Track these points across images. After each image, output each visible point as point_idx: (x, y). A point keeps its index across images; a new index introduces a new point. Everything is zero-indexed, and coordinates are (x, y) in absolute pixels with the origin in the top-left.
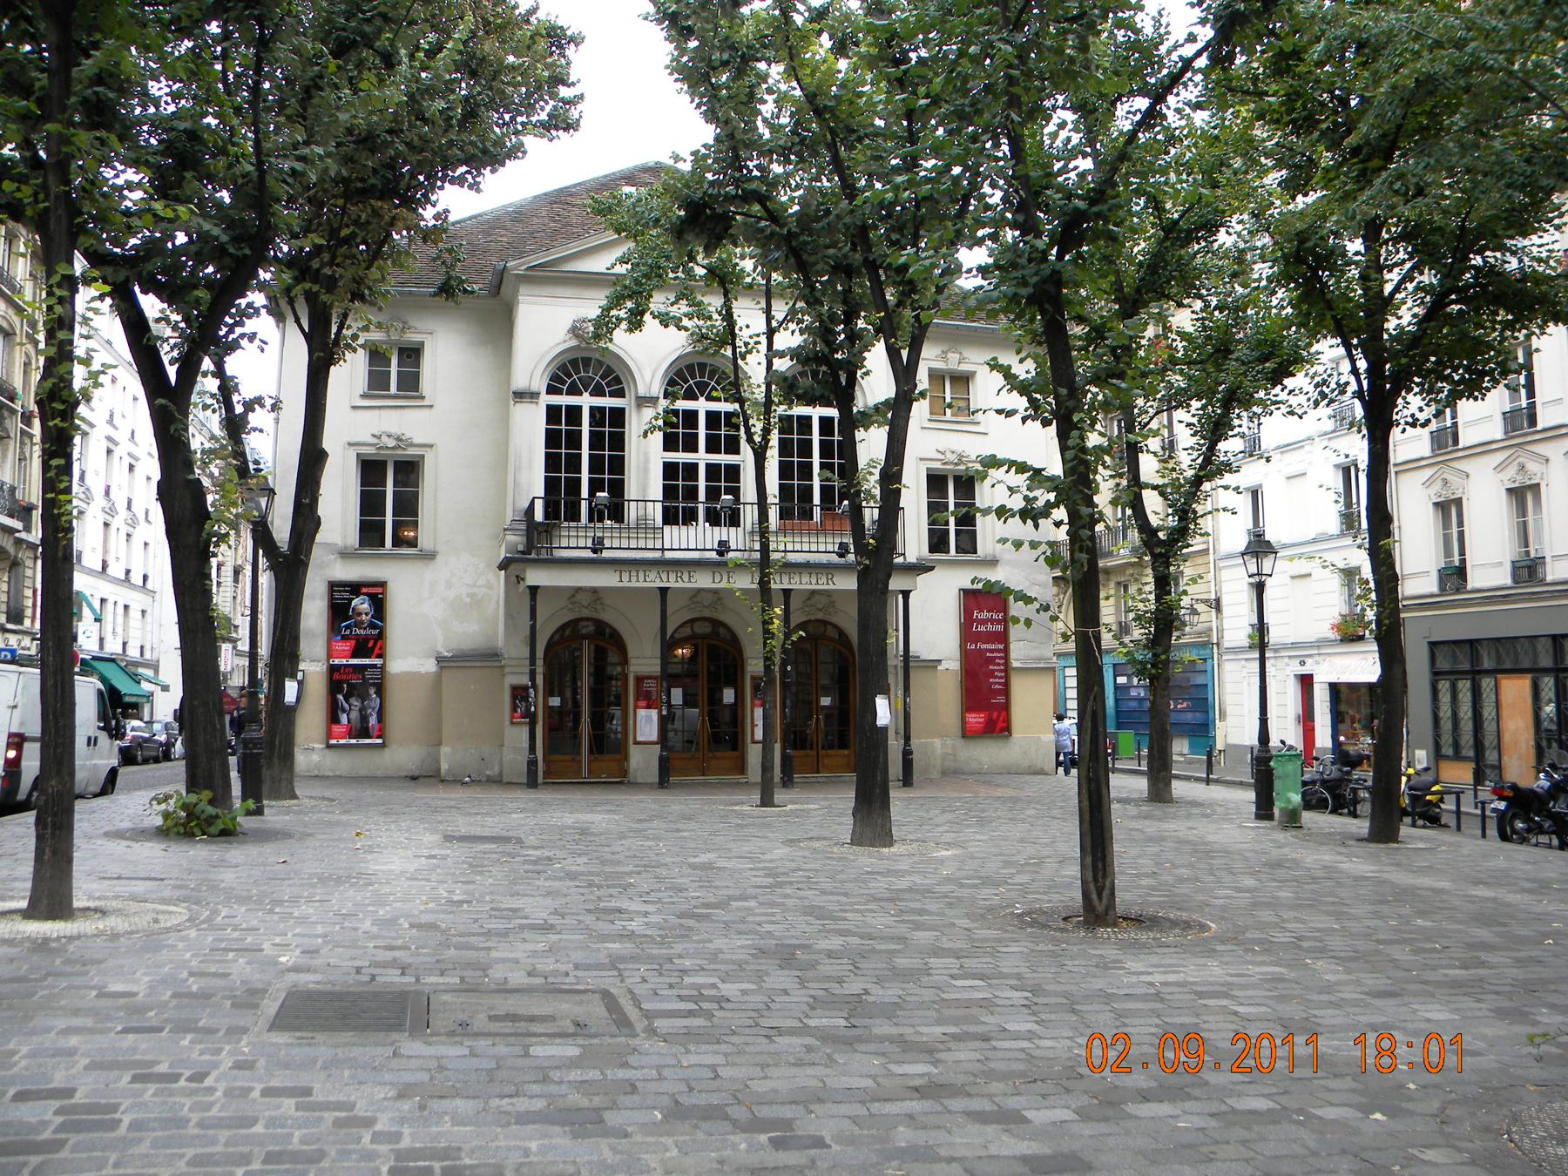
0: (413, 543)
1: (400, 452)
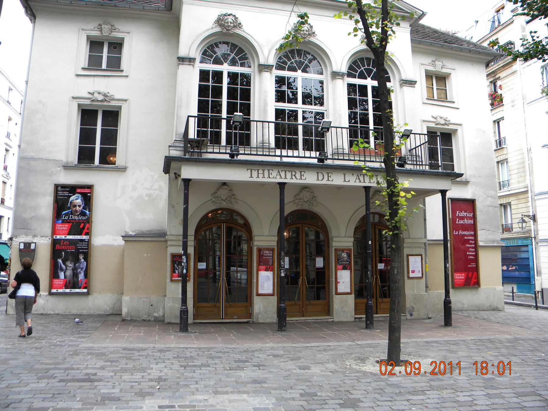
1: (105, 103)
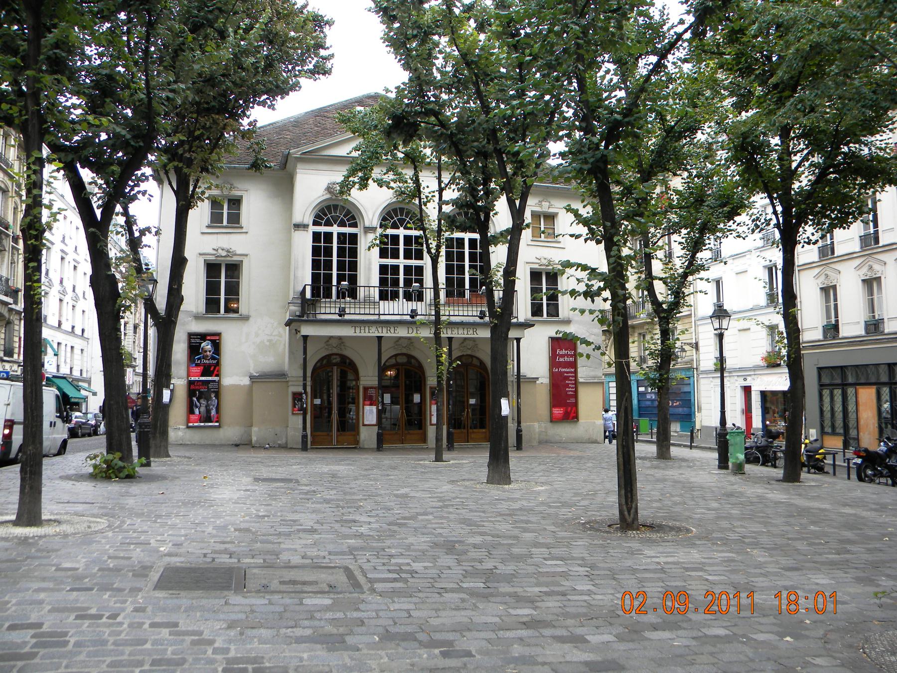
0: (236, 311)
1: (229, 259)
